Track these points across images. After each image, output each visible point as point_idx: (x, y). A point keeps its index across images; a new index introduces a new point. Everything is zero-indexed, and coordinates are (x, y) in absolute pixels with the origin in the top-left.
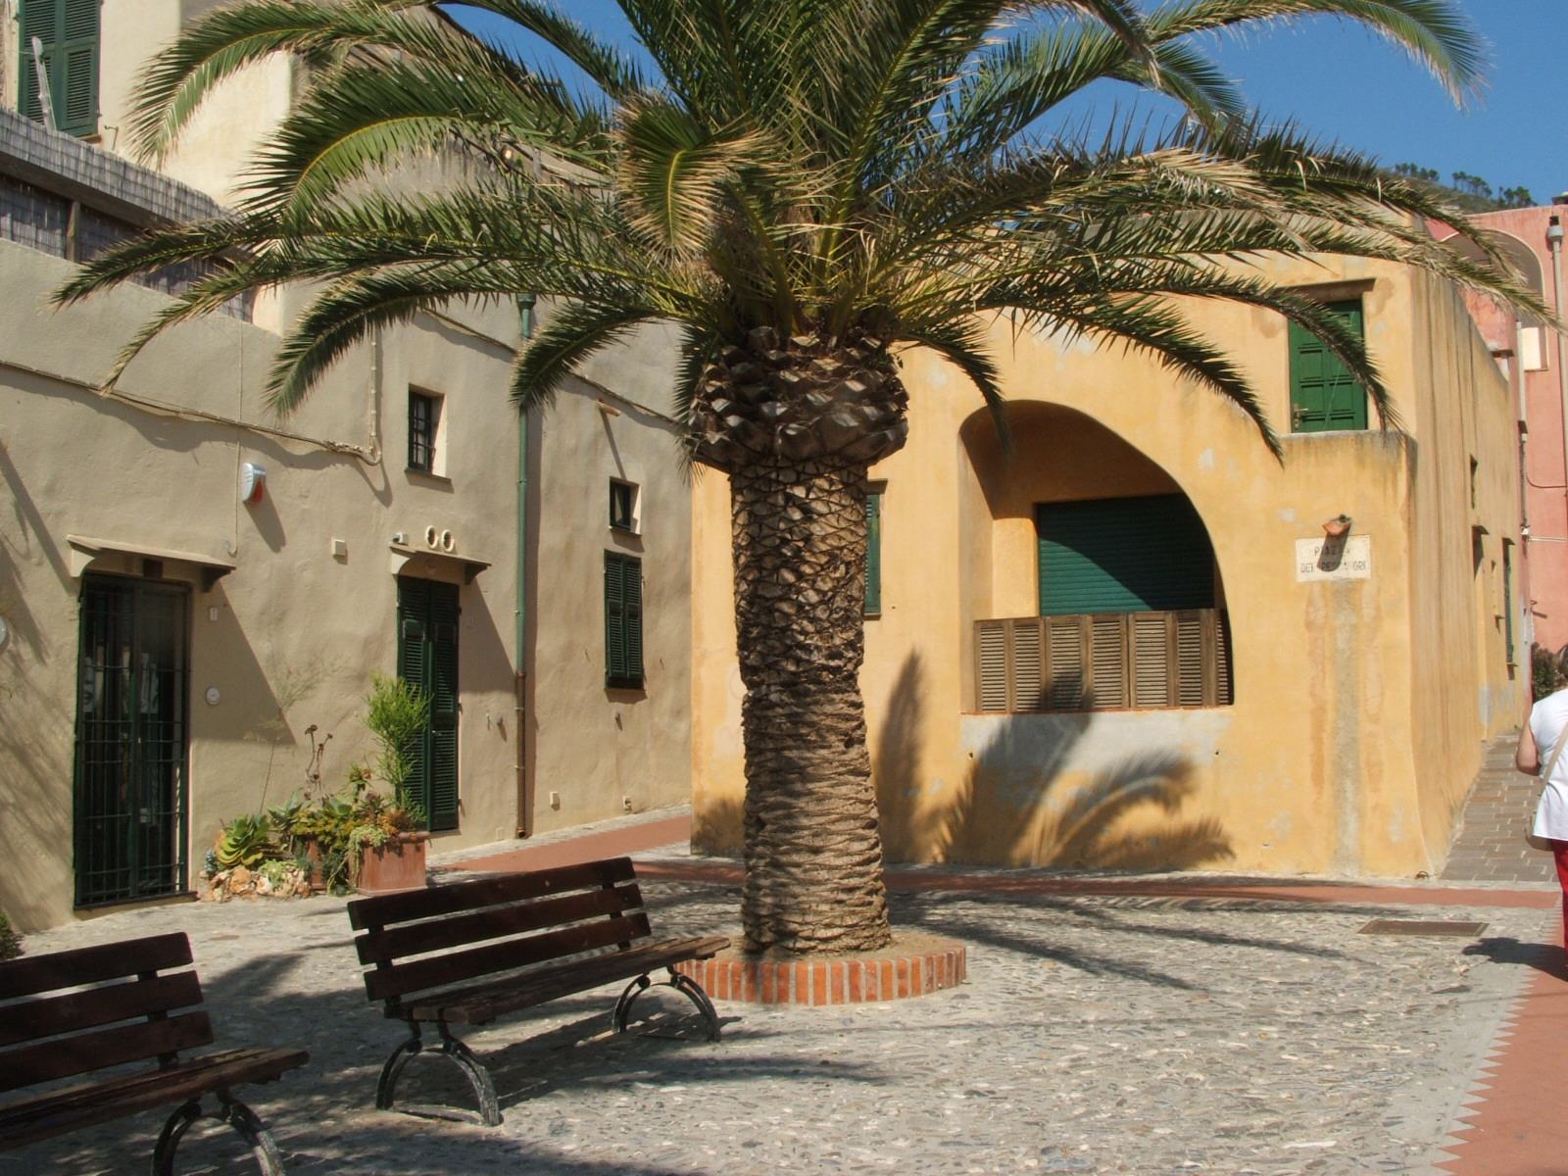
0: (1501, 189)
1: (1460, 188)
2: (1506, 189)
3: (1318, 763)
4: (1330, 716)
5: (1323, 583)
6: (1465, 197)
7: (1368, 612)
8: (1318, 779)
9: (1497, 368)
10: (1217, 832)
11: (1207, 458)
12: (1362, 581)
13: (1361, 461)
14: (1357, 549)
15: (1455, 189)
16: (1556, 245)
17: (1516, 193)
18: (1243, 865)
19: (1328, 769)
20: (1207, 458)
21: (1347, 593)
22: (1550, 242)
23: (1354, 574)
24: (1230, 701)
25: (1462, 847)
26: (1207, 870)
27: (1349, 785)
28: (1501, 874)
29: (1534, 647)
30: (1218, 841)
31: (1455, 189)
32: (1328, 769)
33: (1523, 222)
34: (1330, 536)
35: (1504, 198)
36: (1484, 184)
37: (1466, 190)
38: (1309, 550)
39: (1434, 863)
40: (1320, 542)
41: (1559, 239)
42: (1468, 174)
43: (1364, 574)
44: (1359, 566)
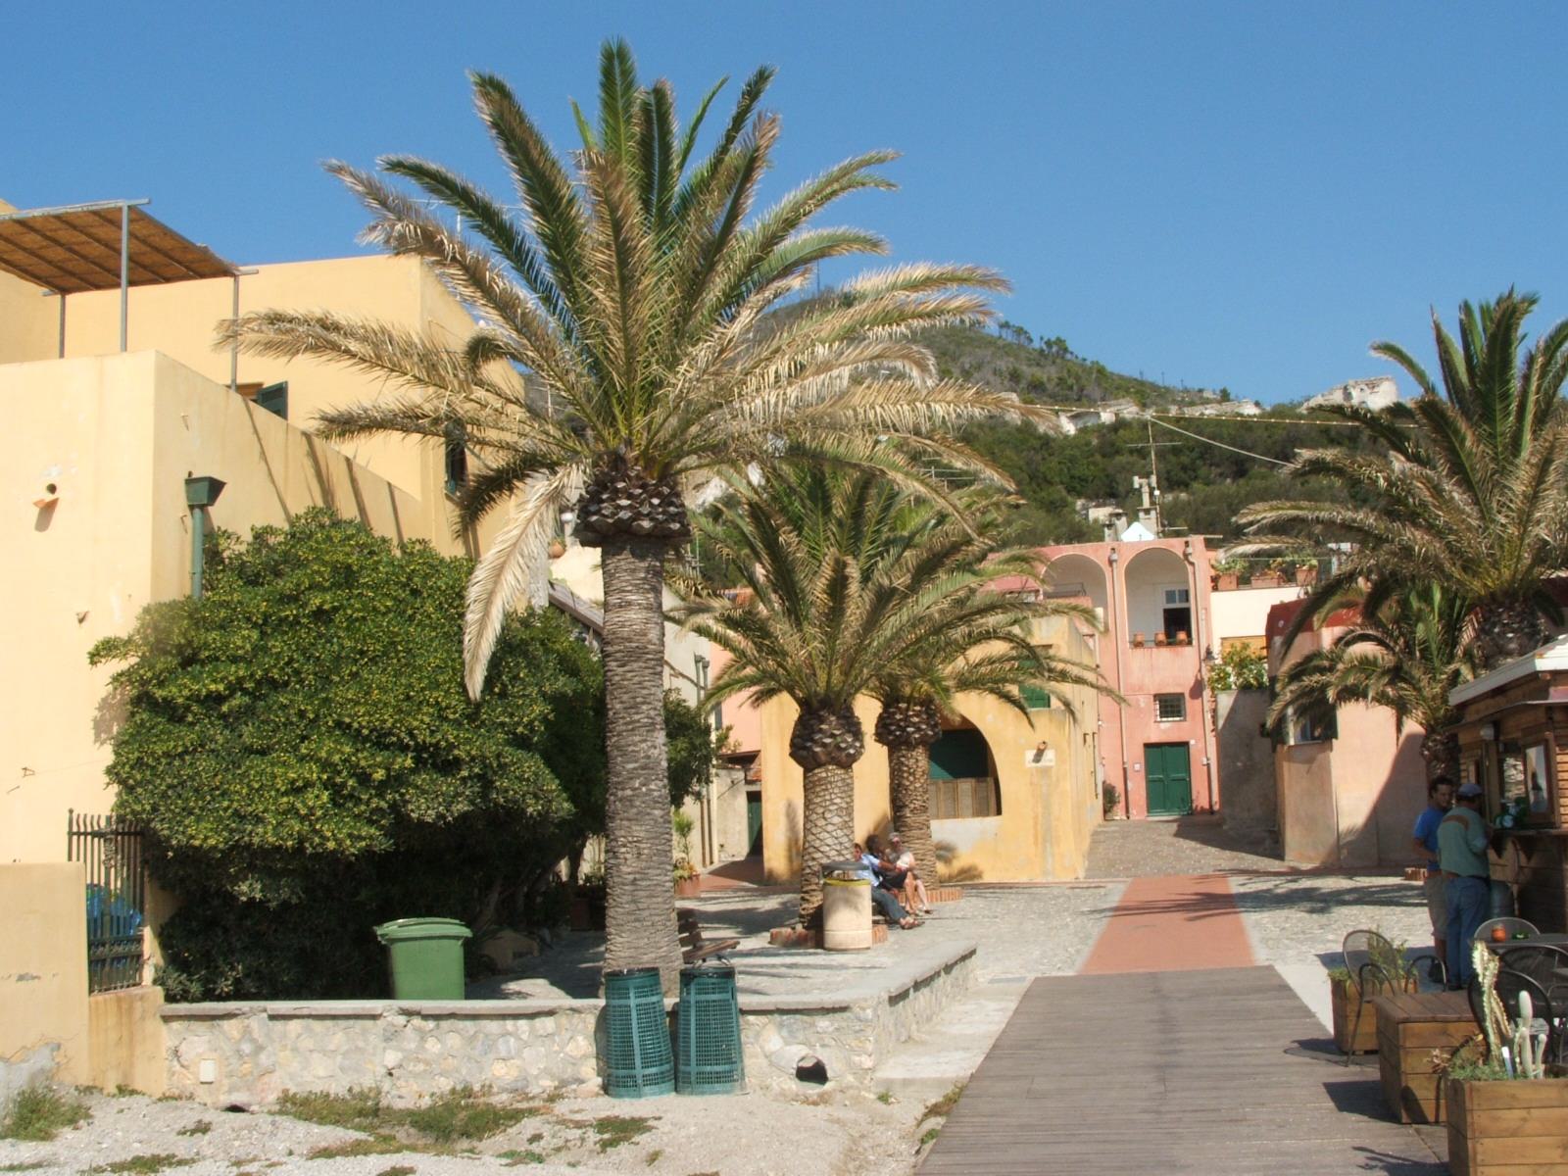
0: (1042, 338)
1: (1004, 336)
2: (1045, 339)
3: (1036, 837)
4: (1040, 818)
5: (1036, 768)
6: (1010, 344)
7: (1054, 779)
8: (1036, 843)
9: (1087, 645)
10: (976, 869)
11: (990, 717)
12: (1051, 767)
13: (1051, 720)
14: (1049, 755)
15: (1000, 337)
16: (1114, 564)
17: (1055, 343)
18: (987, 878)
19: (1040, 840)
20: (990, 717)
21: (1046, 771)
22: (1111, 562)
23: (1048, 764)
24: (999, 812)
25: (1088, 870)
26: (976, 881)
27: (1048, 845)
28: (1106, 876)
29: (1104, 783)
30: (975, 873)
31: (1000, 337)
32: (1040, 840)
33: (1097, 550)
34: (1039, 749)
35: (1045, 347)
36: (1026, 333)
37: (1010, 339)
38: (1031, 754)
39: (1081, 874)
40: (1035, 752)
41: (1116, 561)
42: (1011, 324)
43: (1052, 764)
44: (1051, 761)
